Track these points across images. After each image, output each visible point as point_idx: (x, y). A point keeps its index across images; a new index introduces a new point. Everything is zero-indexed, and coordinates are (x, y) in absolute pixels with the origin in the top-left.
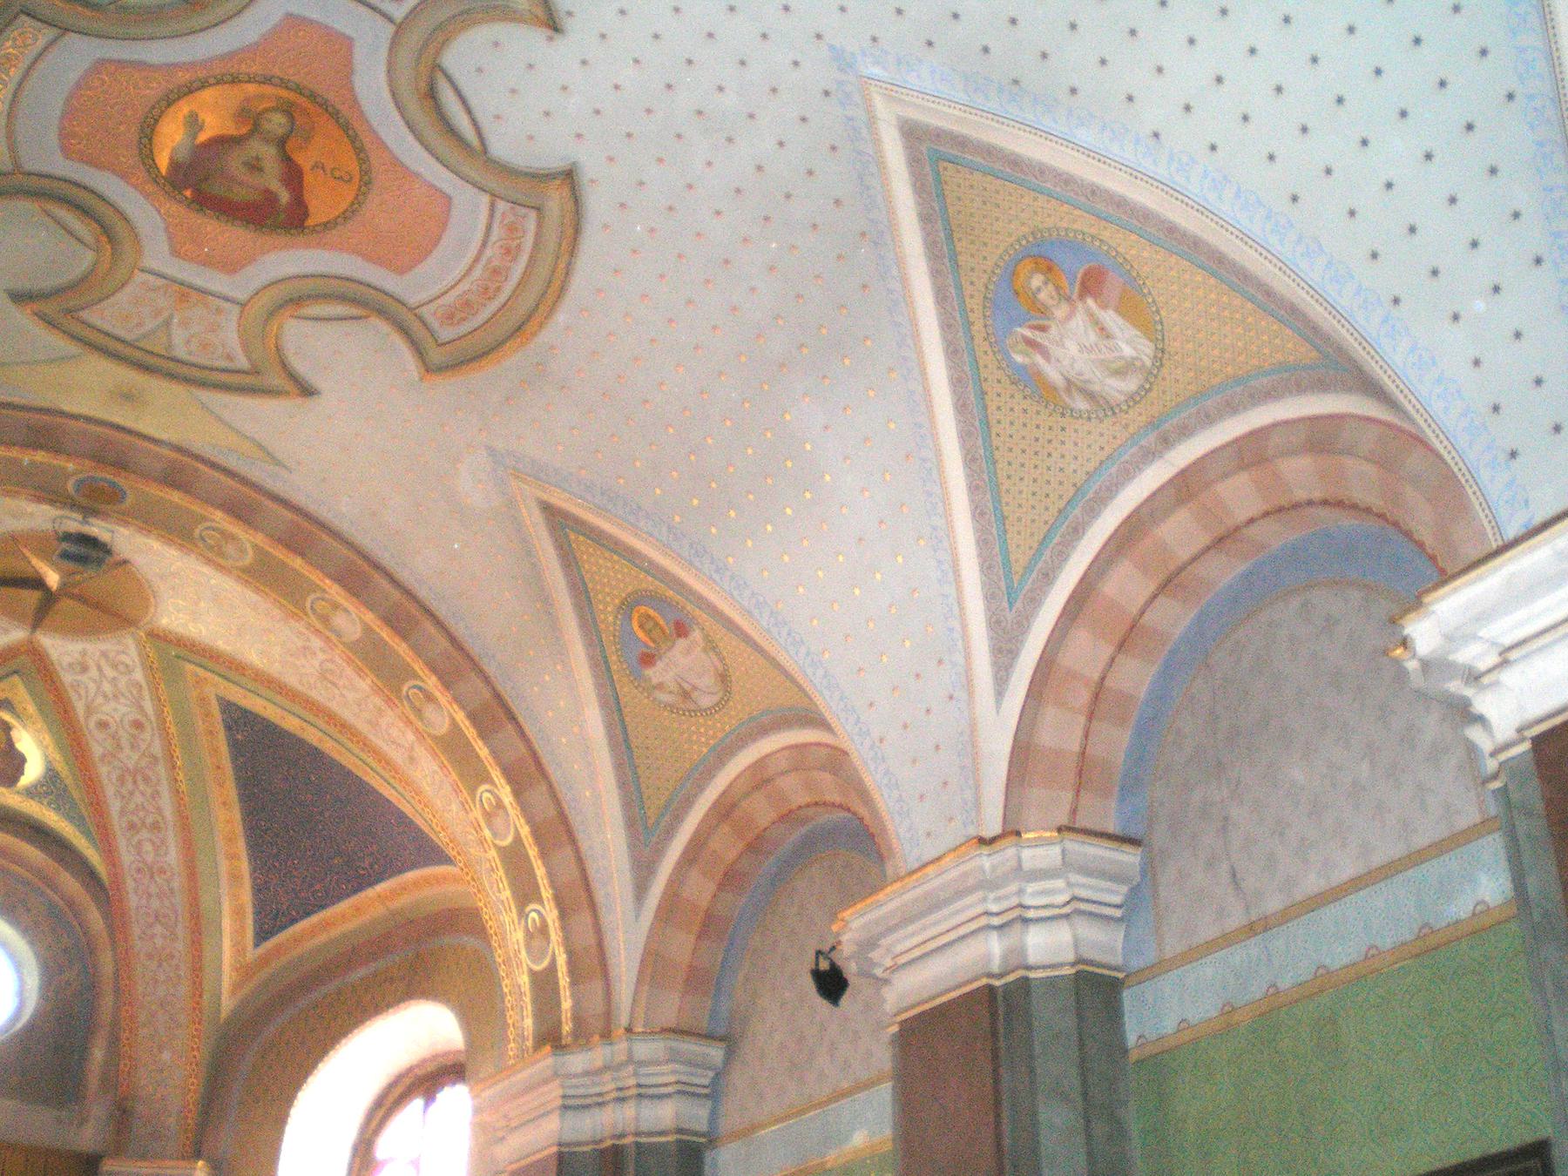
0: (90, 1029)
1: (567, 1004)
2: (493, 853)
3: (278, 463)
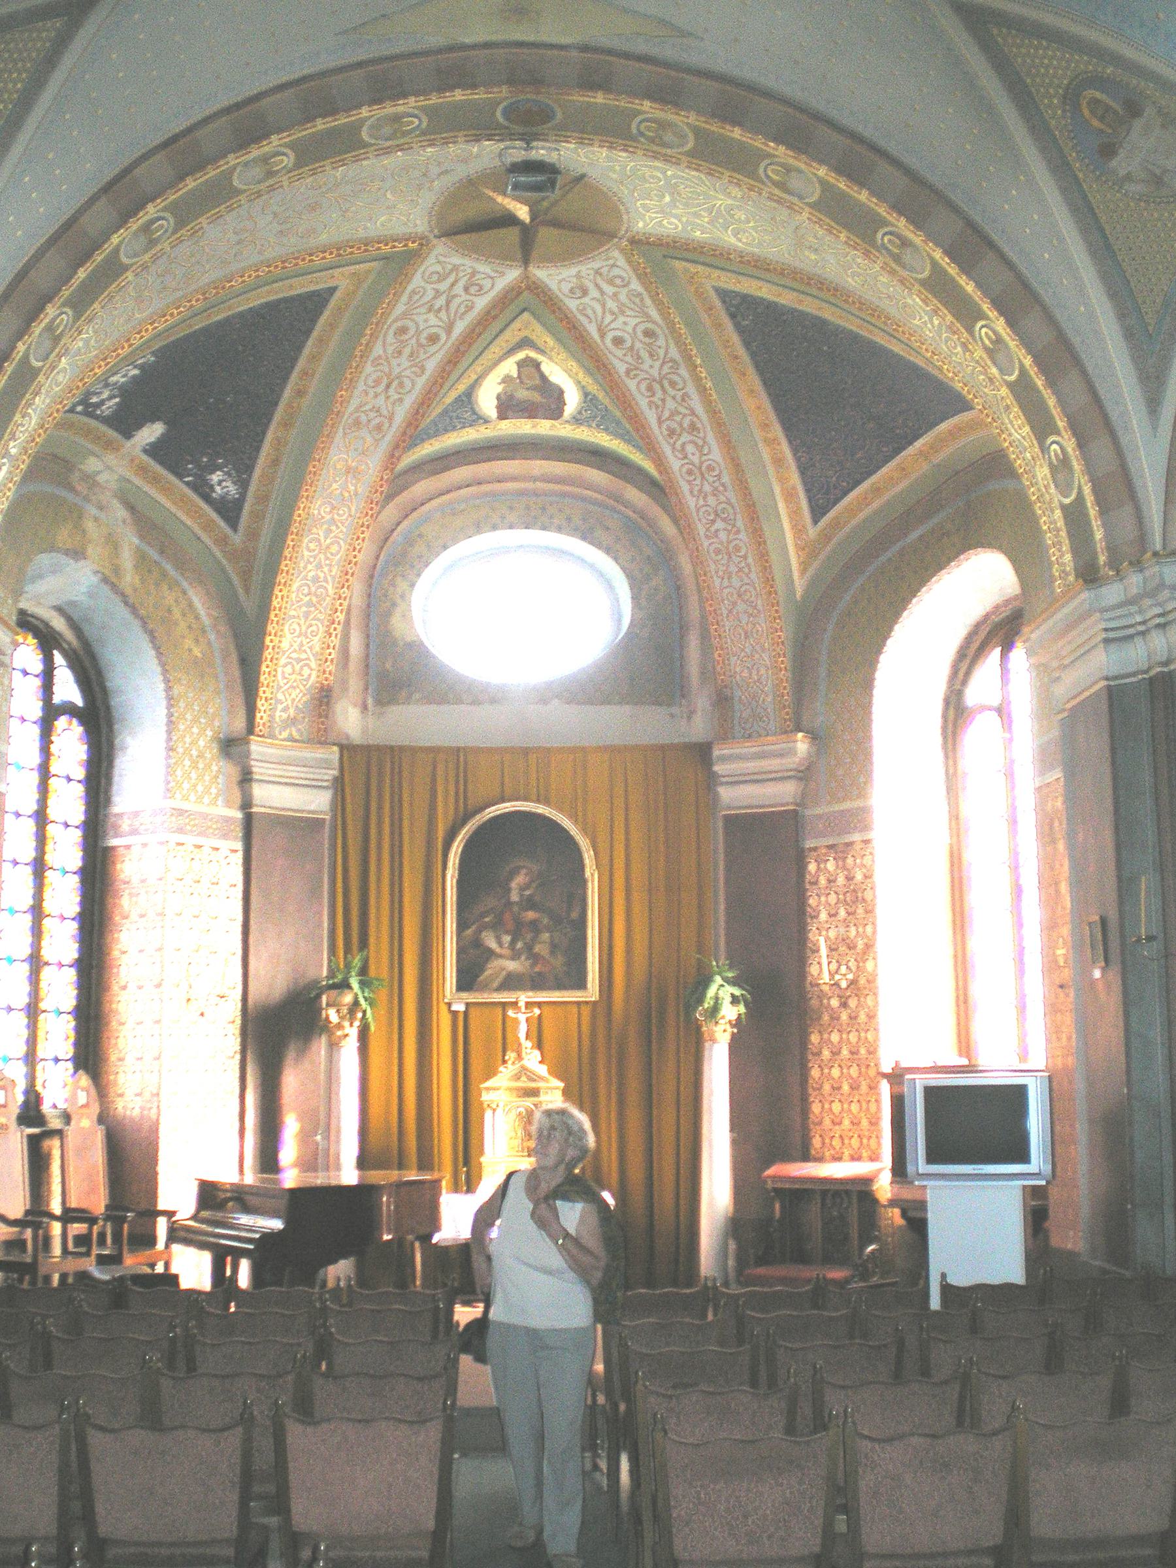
0: (683, 629)
1: (1099, 535)
2: (1004, 391)
3: (684, 34)
